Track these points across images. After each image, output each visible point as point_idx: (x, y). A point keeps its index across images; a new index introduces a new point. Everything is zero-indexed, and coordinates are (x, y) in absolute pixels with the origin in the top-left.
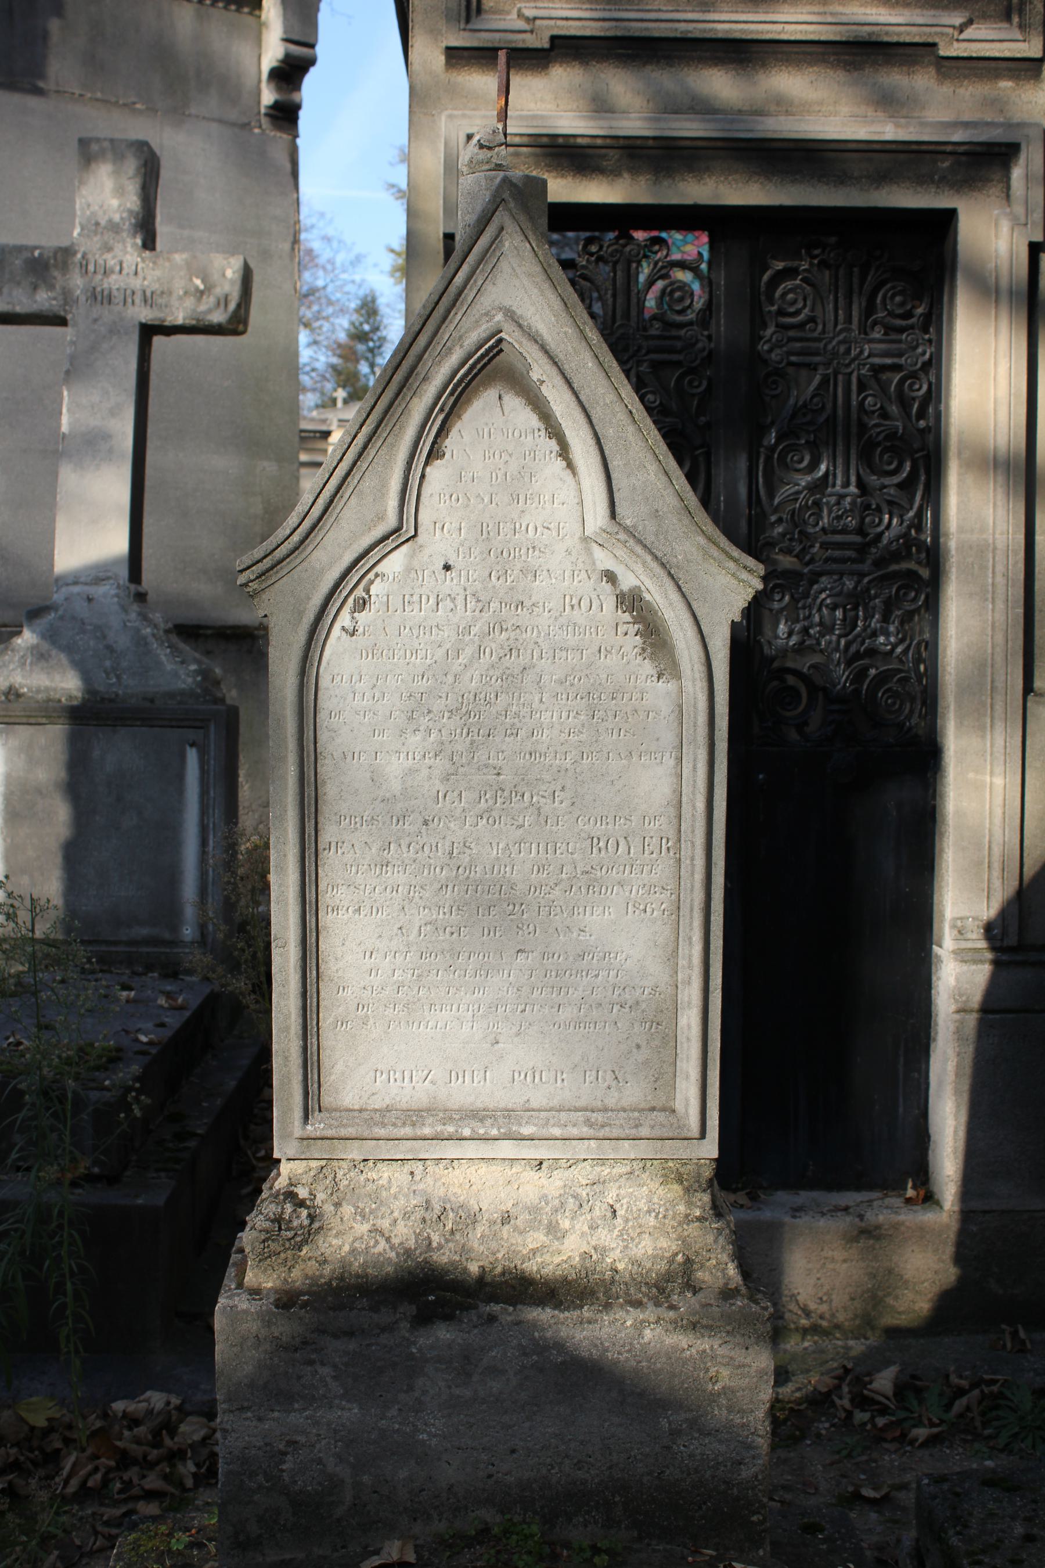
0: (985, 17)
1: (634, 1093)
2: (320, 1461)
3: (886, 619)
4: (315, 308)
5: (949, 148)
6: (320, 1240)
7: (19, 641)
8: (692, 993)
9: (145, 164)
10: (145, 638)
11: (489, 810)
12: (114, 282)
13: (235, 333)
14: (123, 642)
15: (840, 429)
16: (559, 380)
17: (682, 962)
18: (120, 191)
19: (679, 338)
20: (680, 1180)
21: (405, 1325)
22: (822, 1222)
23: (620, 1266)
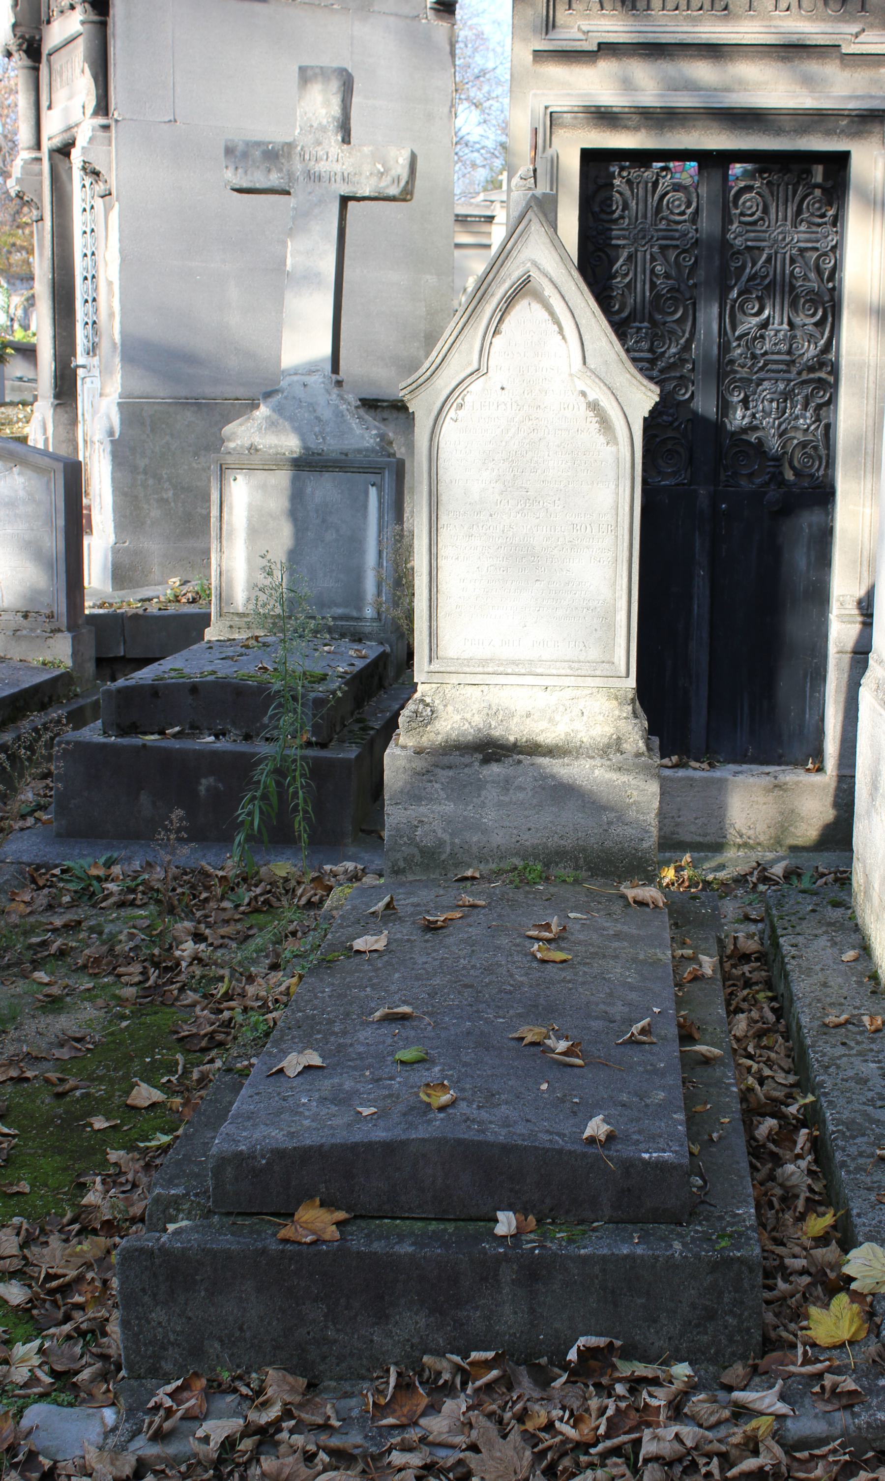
0: (872, 26)
1: (594, 653)
2: (434, 831)
3: (805, 407)
4: (486, 88)
5: (846, 113)
6: (436, 722)
7: (257, 413)
8: (623, 603)
9: (344, 84)
10: (342, 412)
11: (522, 509)
12: (322, 167)
13: (405, 200)
14: (327, 414)
15: (778, 288)
16: (558, 296)
17: (618, 588)
18: (327, 103)
19: (676, 230)
20: (616, 699)
21: (477, 764)
22: (751, 780)
23: (585, 740)
